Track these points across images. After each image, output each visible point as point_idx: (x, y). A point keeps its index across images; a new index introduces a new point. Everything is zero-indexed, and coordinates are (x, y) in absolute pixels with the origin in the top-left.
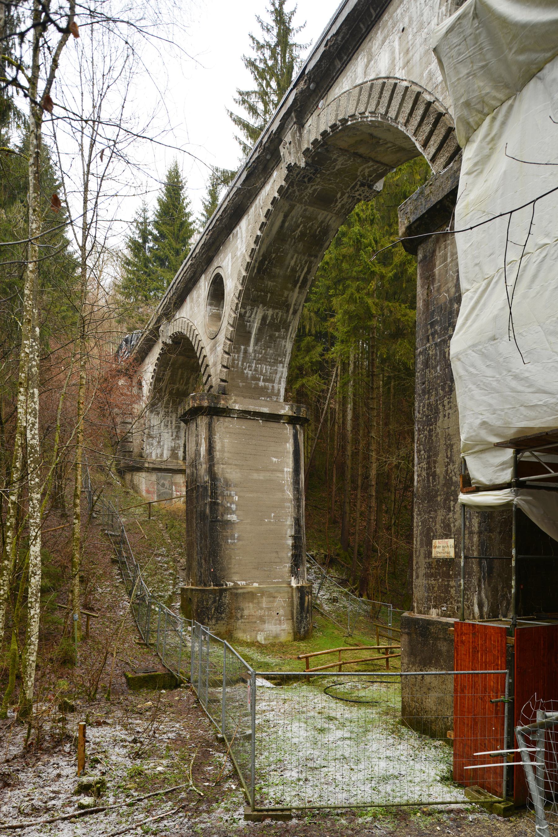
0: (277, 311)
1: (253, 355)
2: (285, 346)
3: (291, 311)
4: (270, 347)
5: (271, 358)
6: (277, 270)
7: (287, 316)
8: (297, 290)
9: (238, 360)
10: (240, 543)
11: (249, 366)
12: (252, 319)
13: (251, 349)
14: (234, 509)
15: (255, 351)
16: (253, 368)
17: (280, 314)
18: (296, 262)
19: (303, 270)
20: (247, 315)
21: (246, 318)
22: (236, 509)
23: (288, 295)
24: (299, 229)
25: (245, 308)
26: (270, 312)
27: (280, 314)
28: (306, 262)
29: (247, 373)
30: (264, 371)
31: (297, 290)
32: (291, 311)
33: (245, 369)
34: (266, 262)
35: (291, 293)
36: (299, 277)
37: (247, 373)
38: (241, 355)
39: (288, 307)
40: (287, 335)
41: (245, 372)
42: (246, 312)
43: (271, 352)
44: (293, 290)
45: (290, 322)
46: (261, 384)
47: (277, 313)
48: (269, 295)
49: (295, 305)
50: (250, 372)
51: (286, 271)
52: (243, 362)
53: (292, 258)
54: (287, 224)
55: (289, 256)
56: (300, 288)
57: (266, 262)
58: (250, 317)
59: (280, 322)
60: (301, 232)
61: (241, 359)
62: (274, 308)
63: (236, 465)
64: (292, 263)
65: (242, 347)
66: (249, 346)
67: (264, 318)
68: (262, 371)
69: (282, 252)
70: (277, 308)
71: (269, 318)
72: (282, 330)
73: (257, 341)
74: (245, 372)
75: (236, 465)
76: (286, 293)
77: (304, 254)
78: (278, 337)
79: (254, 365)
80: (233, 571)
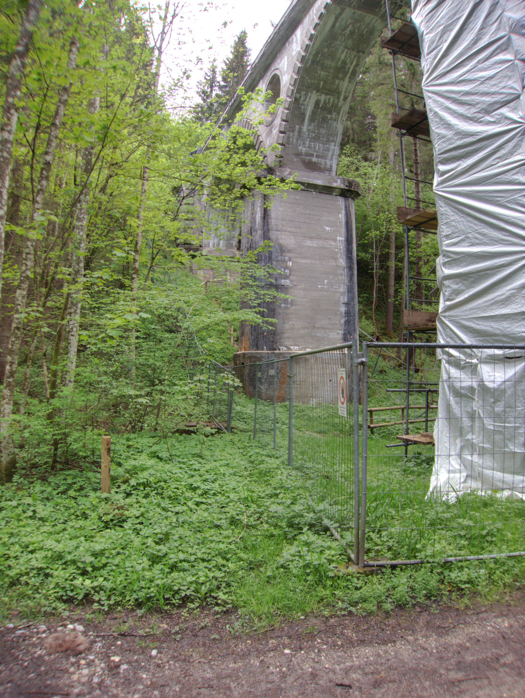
0: (329, 97)
1: (307, 133)
2: (336, 127)
3: (342, 97)
4: (323, 127)
5: (323, 137)
6: (328, 63)
7: (338, 102)
8: (347, 79)
9: (293, 138)
10: (293, 308)
11: (303, 143)
12: (306, 103)
13: (305, 128)
14: (288, 274)
15: (308, 130)
16: (307, 145)
17: (332, 99)
18: (346, 56)
19: (352, 63)
20: (302, 99)
21: (301, 102)
22: (290, 274)
23: (339, 84)
24: (349, 29)
25: (300, 94)
26: (323, 98)
27: (332, 99)
28: (355, 56)
29: (301, 150)
30: (317, 148)
31: (347, 79)
32: (342, 97)
33: (300, 146)
34: (320, 56)
35: (341, 82)
36: (349, 68)
37: (301, 150)
38: (296, 133)
39: (339, 93)
40: (338, 118)
41: (300, 148)
42: (300, 97)
43: (324, 131)
44: (343, 79)
45: (341, 107)
46: (314, 159)
47: (329, 99)
48: (322, 83)
49: (345, 92)
50: (304, 149)
51: (337, 63)
52: (297, 140)
53: (343, 52)
54: (337, 24)
55: (340, 51)
56: (350, 78)
57: (320, 56)
58: (304, 101)
59: (332, 106)
60: (350, 31)
61: (296, 136)
62: (326, 94)
63: (290, 232)
64: (343, 57)
65: (297, 127)
66: (303, 125)
67: (317, 103)
68: (315, 148)
69: (333, 47)
70: (329, 94)
71: (322, 102)
72: (334, 114)
73: (312, 120)
74: (300, 148)
75: (290, 232)
76: (337, 82)
77: (353, 50)
78: (331, 119)
79: (308, 143)
80: (286, 335)
